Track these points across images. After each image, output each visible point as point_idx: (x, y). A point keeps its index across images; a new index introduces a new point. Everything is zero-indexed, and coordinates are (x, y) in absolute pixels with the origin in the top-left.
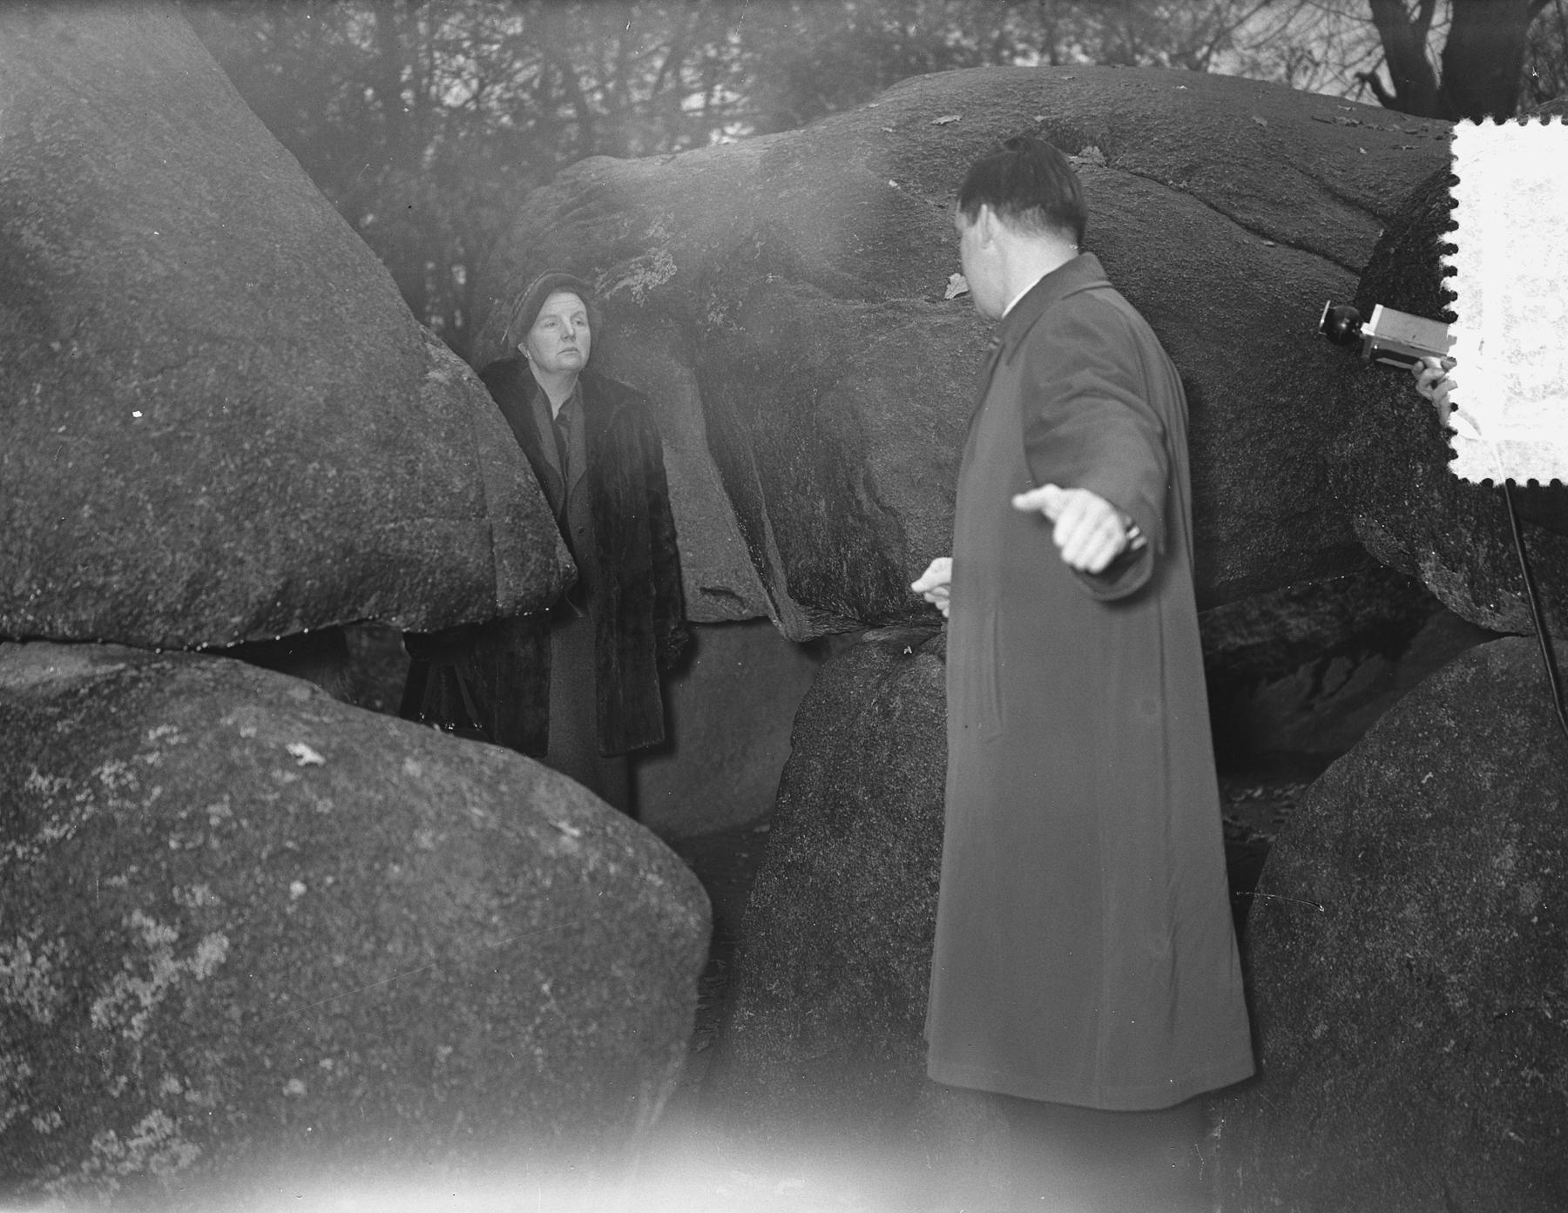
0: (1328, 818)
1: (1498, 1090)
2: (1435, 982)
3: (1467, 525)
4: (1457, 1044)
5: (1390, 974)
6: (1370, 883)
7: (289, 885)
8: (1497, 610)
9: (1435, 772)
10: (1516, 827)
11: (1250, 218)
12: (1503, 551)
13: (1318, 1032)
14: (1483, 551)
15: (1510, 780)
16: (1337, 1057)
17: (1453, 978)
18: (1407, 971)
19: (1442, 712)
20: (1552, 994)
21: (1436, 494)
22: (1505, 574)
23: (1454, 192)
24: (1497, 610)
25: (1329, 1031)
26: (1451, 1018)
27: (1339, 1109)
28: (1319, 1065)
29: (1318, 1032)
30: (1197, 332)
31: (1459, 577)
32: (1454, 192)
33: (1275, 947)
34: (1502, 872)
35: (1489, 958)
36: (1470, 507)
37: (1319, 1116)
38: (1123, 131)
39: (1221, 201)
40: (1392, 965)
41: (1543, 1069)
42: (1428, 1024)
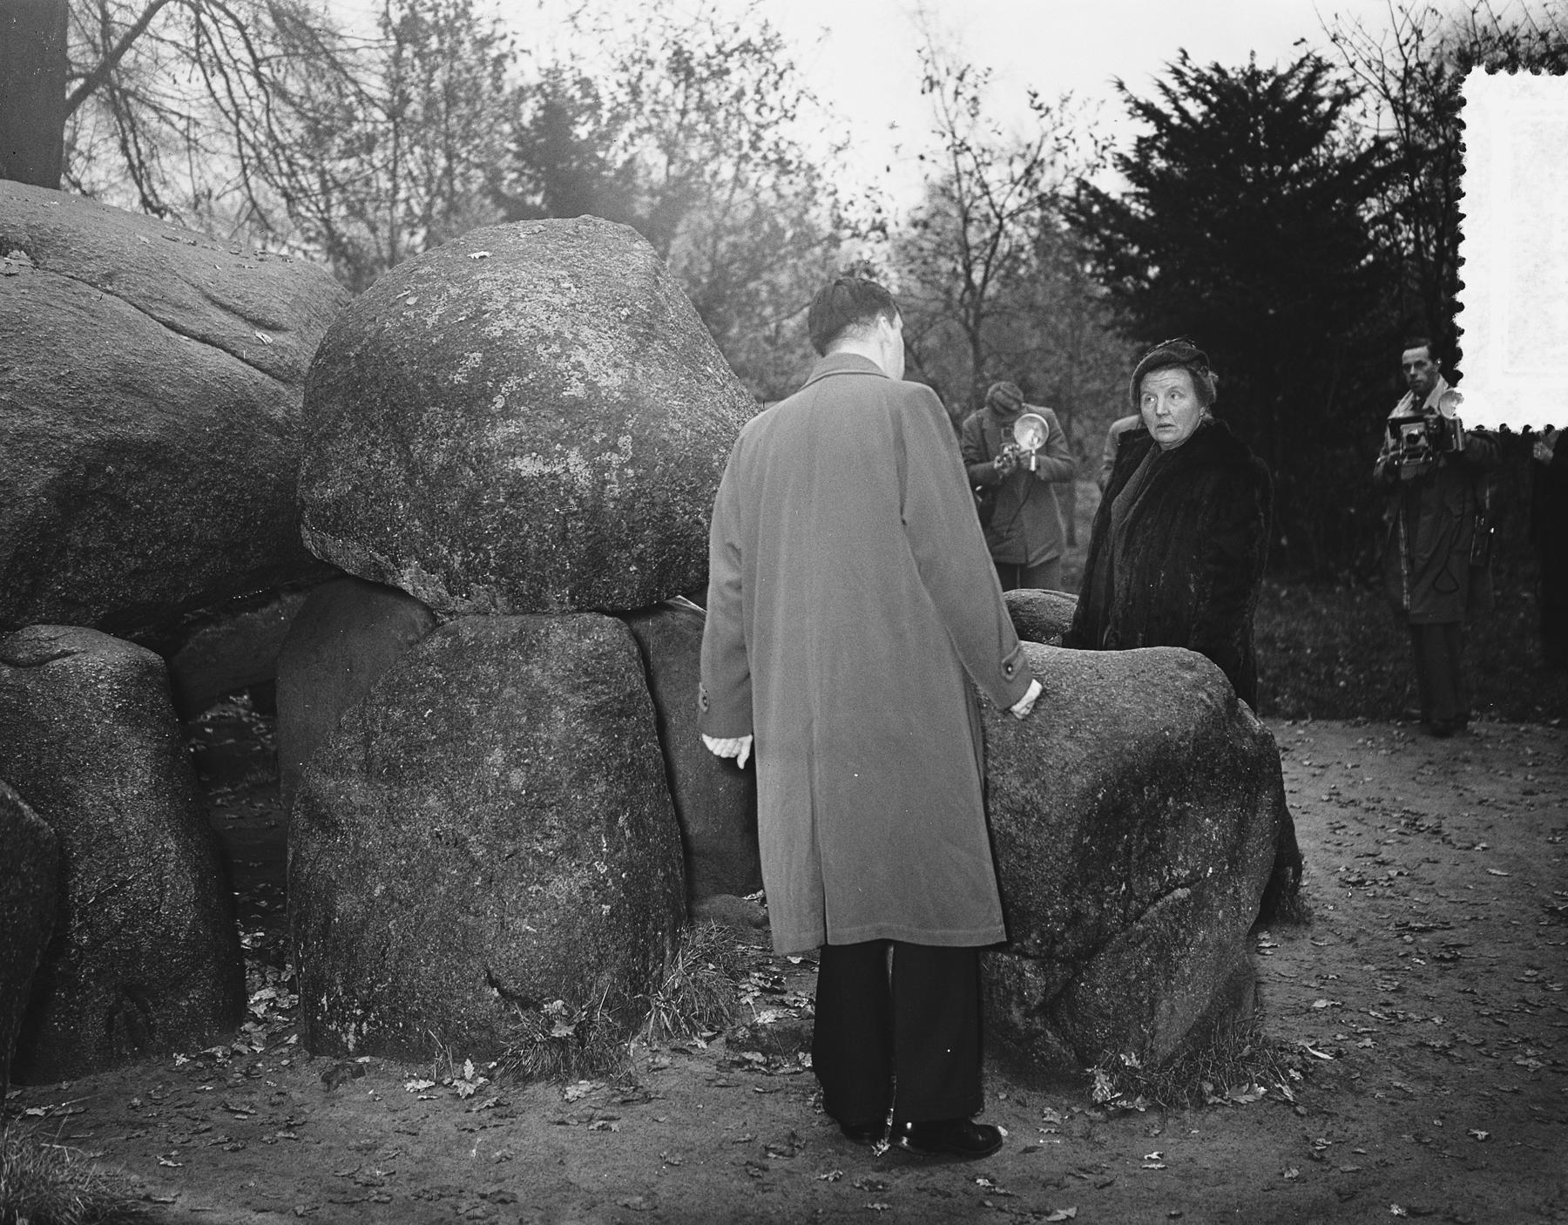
0: (350, 750)
1: (516, 902)
2: (459, 843)
3: (443, 542)
4: (483, 879)
5: (425, 843)
6: (396, 789)
7: (1046, 403)
8: (467, 598)
9: (433, 708)
10: (499, 736)
11: (168, 317)
12: (475, 558)
13: (377, 892)
14: (458, 559)
15: (490, 707)
16: (396, 904)
17: (473, 838)
18: (438, 840)
19: (431, 669)
20: (539, 837)
21: (417, 522)
22: (477, 574)
23: (1460, 297)
24: (467, 598)
25: (387, 889)
26: (475, 863)
27: (404, 938)
28: (382, 912)
29: (377, 892)
30: (156, 405)
31: (435, 577)
32: (1460, 297)
33: (326, 843)
34: (495, 766)
35: (496, 821)
36: (445, 530)
37: (389, 945)
38: (42, 240)
39: (140, 302)
40: (426, 837)
41: (542, 884)
42: (461, 870)
